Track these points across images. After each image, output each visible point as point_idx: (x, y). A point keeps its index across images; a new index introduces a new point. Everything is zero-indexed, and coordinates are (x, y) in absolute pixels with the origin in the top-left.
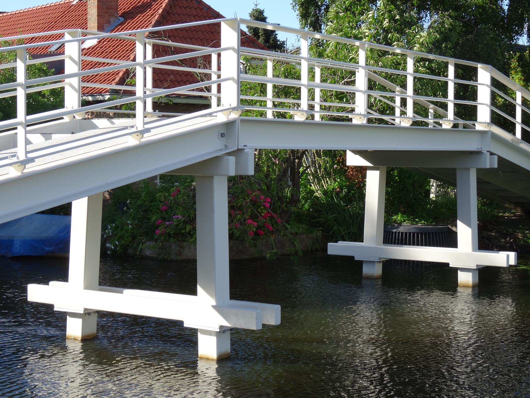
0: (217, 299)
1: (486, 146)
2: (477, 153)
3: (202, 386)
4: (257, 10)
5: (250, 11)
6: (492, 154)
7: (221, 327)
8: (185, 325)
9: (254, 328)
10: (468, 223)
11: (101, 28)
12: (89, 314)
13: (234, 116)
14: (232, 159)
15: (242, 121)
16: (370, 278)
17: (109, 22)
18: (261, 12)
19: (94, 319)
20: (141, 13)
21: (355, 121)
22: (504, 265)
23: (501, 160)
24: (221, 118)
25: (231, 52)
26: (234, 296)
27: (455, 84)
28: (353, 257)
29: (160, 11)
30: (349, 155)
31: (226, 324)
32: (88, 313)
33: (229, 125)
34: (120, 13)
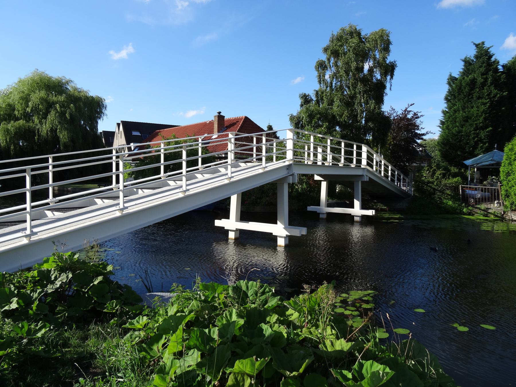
0: (285, 225)
1: (365, 173)
2: (362, 176)
3: (279, 254)
4: (269, 125)
5: (267, 126)
6: (367, 176)
7: (286, 235)
8: (273, 234)
9: (299, 236)
10: (358, 200)
11: (219, 132)
12: (237, 230)
13: (291, 162)
14: (291, 177)
15: (294, 164)
16: (323, 219)
17: (221, 130)
18: (271, 126)
19: (238, 232)
20: (233, 126)
21: (340, 165)
22: (371, 215)
23: (370, 178)
24: (287, 163)
25: (290, 140)
26: (289, 225)
27: (356, 151)
28: (316, 212)
29: (240, 126)
30: (315, 175)
31: (288, 234)
32: (237, 230)
33: (289, 166)
34: (225, 126)
